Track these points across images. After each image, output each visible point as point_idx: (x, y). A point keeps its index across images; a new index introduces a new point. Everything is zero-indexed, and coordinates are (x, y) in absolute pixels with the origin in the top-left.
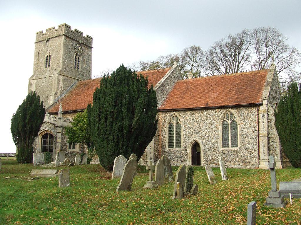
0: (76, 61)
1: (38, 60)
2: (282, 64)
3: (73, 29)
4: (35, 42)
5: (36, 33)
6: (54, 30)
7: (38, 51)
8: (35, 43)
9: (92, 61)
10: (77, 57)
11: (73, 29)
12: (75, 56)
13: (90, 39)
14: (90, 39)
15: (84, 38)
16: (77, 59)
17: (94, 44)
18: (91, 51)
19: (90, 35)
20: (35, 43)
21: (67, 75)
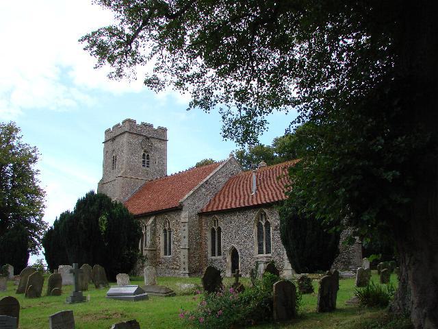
3: (139, 123)
10: (146, 154)
11: (139, 123)
13: (163, 131)
14: (163, 131)
16: (146, 157)
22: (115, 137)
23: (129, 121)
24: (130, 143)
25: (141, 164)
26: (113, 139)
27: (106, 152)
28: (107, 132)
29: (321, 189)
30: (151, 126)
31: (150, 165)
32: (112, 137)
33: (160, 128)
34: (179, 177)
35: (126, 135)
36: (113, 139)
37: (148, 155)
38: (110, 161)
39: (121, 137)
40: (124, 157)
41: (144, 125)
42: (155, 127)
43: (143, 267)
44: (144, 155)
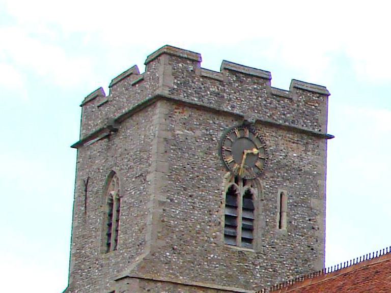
0: (232, 205)
1: (85, 221)
2: (120, 288)
3: (211, 63)
4: (77, 139)
5: (81, 100)
6: (133, 80)
7: (85, 178)
8: (331, 137)
9: (324, 197)
10: (241, 190)
11: (211, 63)
12: (225, 186)
13: (313, 97)
14: (313, 97)
15: (279, 95)
16: (240, 202)
17: (338, 118)
18: (322, 156)
19: (311, 77)
20: (331, 137)
21: (181, 279)
22: (120, 121)
23: (169, 54)
24: (173, 144)
25: (218, 233)
26: (110, 131)
27: (84, 186)
28: (92, 101)
29: (84, 274)
30: (263, 78)
31: (257, 235)
32: (107, 123)
33: (298, 87)
34: (343, 273)
35: (160, 111)
36: (110, 131)
37: (248, 195)
38: (97, 219)
39: (140, 118)
40: (147, 204)
41: (235, 73)
42: (281, 82)
43: (292, 135)
44: (232, 193)
